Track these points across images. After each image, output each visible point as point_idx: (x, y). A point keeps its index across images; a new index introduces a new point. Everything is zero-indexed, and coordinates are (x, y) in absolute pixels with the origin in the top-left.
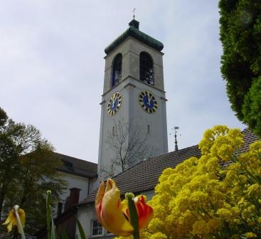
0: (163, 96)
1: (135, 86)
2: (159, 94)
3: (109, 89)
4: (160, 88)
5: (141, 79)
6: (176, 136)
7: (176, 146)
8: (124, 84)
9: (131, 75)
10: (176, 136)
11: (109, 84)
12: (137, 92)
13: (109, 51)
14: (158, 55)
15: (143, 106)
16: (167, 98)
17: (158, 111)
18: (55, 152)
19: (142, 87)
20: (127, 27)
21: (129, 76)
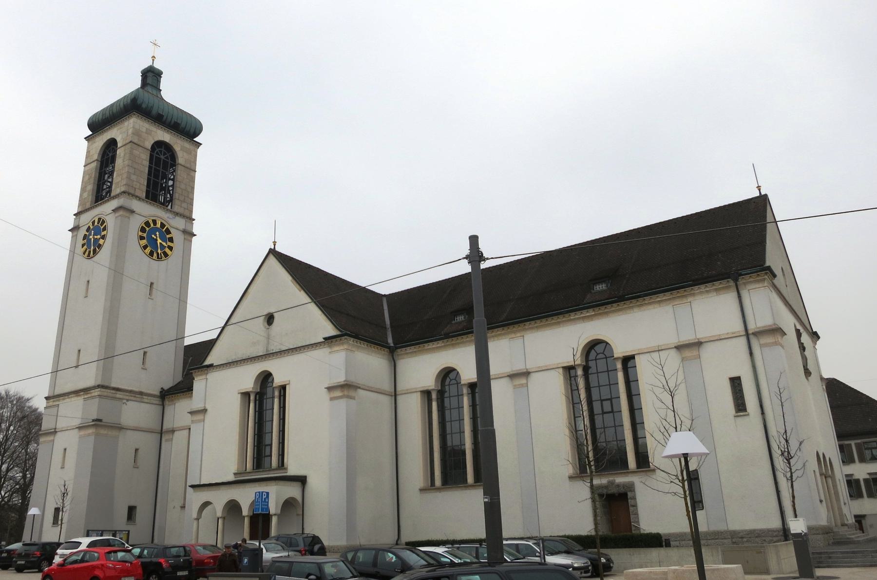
0: (188, 229)
1: (133, 212)
2: (179, 223)
3: (88, 205)
4: (187, 213)
5: (147, 197)
6: (256, 333)
7: (605, 439)
8: (113, 204)
9: (136, 141)
10: (256, 333)
11: (89, 197)
12: (136, 222)
13: (97, 125)
14: (187, 145)
15: (145, 247)
16: (195, 231)
17: (175, 256)
18: (645, 532)
19: (147, 211)
20: (134, 83)
21: (131, 142)
